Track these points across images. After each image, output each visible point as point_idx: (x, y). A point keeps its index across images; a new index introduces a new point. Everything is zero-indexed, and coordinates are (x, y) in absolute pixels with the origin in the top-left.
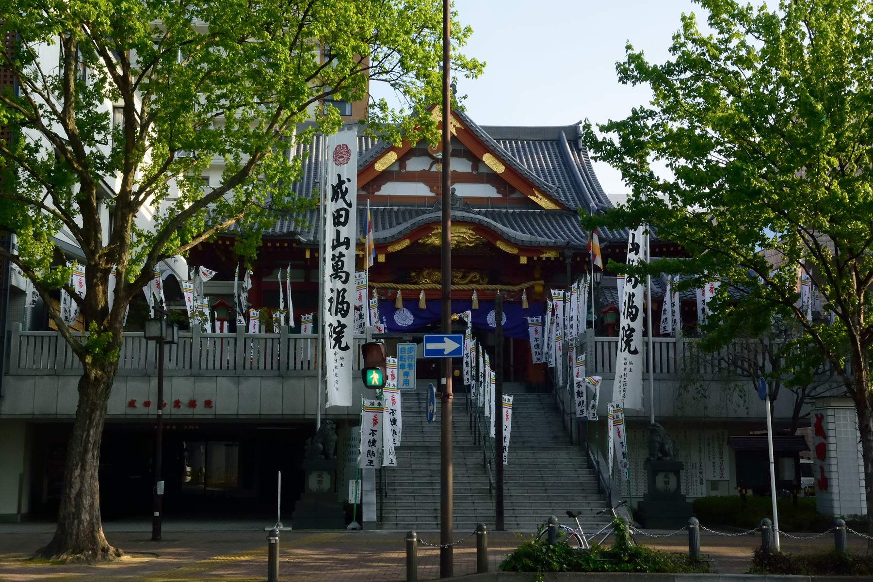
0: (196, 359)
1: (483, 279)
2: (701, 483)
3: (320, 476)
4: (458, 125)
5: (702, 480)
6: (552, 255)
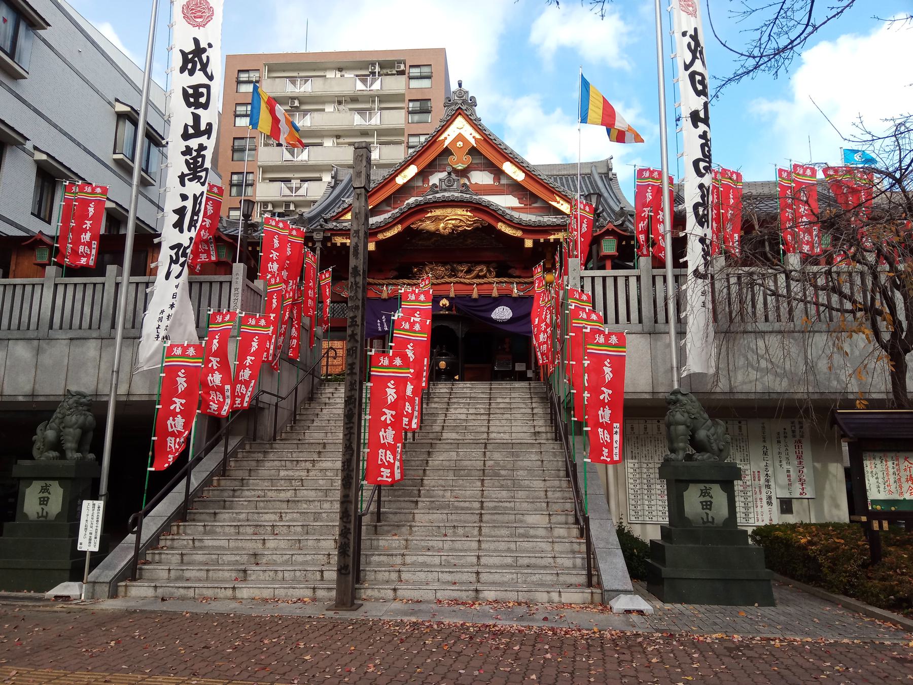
0: (25, 319)
1: (490, 272)
2: (770, 503)
3: (45, 489)
4: (478, 136)
5: (770, 497)
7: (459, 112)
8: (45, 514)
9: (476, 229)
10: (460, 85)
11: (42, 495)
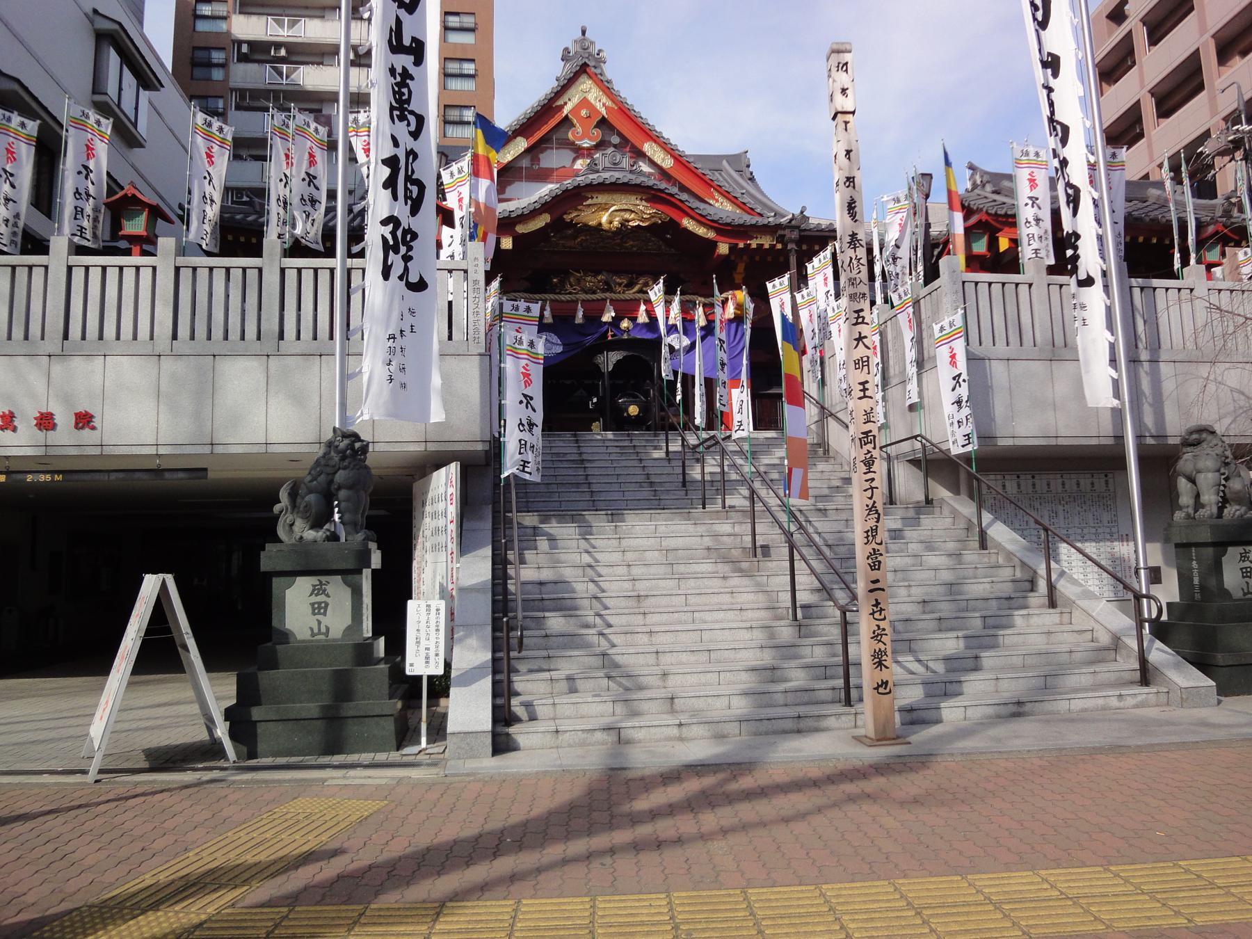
4: (609, 103)
6: (767, 242)
7: (583, 69)
8: (323, 630)
9: (654, 225)
10: (584, 33)
11: (314, 599)
